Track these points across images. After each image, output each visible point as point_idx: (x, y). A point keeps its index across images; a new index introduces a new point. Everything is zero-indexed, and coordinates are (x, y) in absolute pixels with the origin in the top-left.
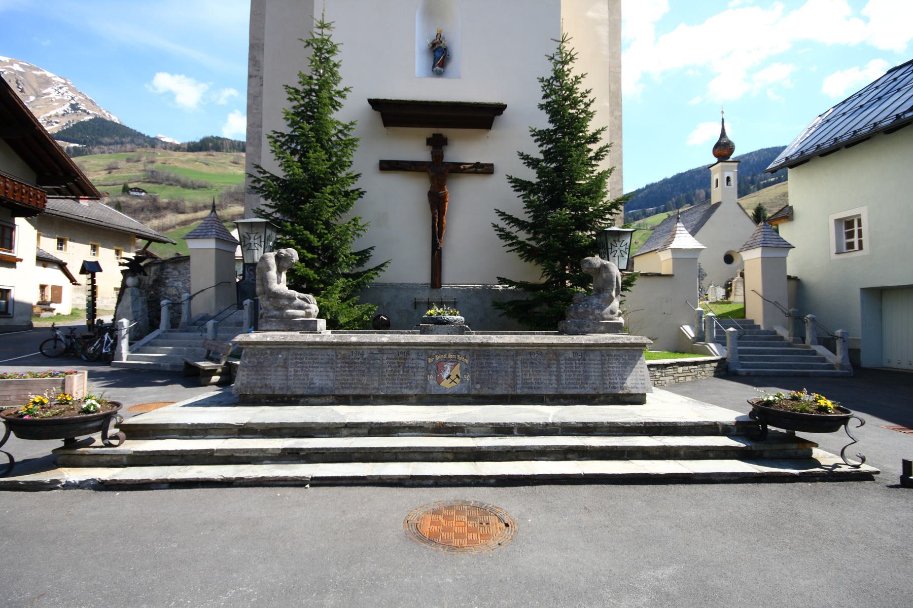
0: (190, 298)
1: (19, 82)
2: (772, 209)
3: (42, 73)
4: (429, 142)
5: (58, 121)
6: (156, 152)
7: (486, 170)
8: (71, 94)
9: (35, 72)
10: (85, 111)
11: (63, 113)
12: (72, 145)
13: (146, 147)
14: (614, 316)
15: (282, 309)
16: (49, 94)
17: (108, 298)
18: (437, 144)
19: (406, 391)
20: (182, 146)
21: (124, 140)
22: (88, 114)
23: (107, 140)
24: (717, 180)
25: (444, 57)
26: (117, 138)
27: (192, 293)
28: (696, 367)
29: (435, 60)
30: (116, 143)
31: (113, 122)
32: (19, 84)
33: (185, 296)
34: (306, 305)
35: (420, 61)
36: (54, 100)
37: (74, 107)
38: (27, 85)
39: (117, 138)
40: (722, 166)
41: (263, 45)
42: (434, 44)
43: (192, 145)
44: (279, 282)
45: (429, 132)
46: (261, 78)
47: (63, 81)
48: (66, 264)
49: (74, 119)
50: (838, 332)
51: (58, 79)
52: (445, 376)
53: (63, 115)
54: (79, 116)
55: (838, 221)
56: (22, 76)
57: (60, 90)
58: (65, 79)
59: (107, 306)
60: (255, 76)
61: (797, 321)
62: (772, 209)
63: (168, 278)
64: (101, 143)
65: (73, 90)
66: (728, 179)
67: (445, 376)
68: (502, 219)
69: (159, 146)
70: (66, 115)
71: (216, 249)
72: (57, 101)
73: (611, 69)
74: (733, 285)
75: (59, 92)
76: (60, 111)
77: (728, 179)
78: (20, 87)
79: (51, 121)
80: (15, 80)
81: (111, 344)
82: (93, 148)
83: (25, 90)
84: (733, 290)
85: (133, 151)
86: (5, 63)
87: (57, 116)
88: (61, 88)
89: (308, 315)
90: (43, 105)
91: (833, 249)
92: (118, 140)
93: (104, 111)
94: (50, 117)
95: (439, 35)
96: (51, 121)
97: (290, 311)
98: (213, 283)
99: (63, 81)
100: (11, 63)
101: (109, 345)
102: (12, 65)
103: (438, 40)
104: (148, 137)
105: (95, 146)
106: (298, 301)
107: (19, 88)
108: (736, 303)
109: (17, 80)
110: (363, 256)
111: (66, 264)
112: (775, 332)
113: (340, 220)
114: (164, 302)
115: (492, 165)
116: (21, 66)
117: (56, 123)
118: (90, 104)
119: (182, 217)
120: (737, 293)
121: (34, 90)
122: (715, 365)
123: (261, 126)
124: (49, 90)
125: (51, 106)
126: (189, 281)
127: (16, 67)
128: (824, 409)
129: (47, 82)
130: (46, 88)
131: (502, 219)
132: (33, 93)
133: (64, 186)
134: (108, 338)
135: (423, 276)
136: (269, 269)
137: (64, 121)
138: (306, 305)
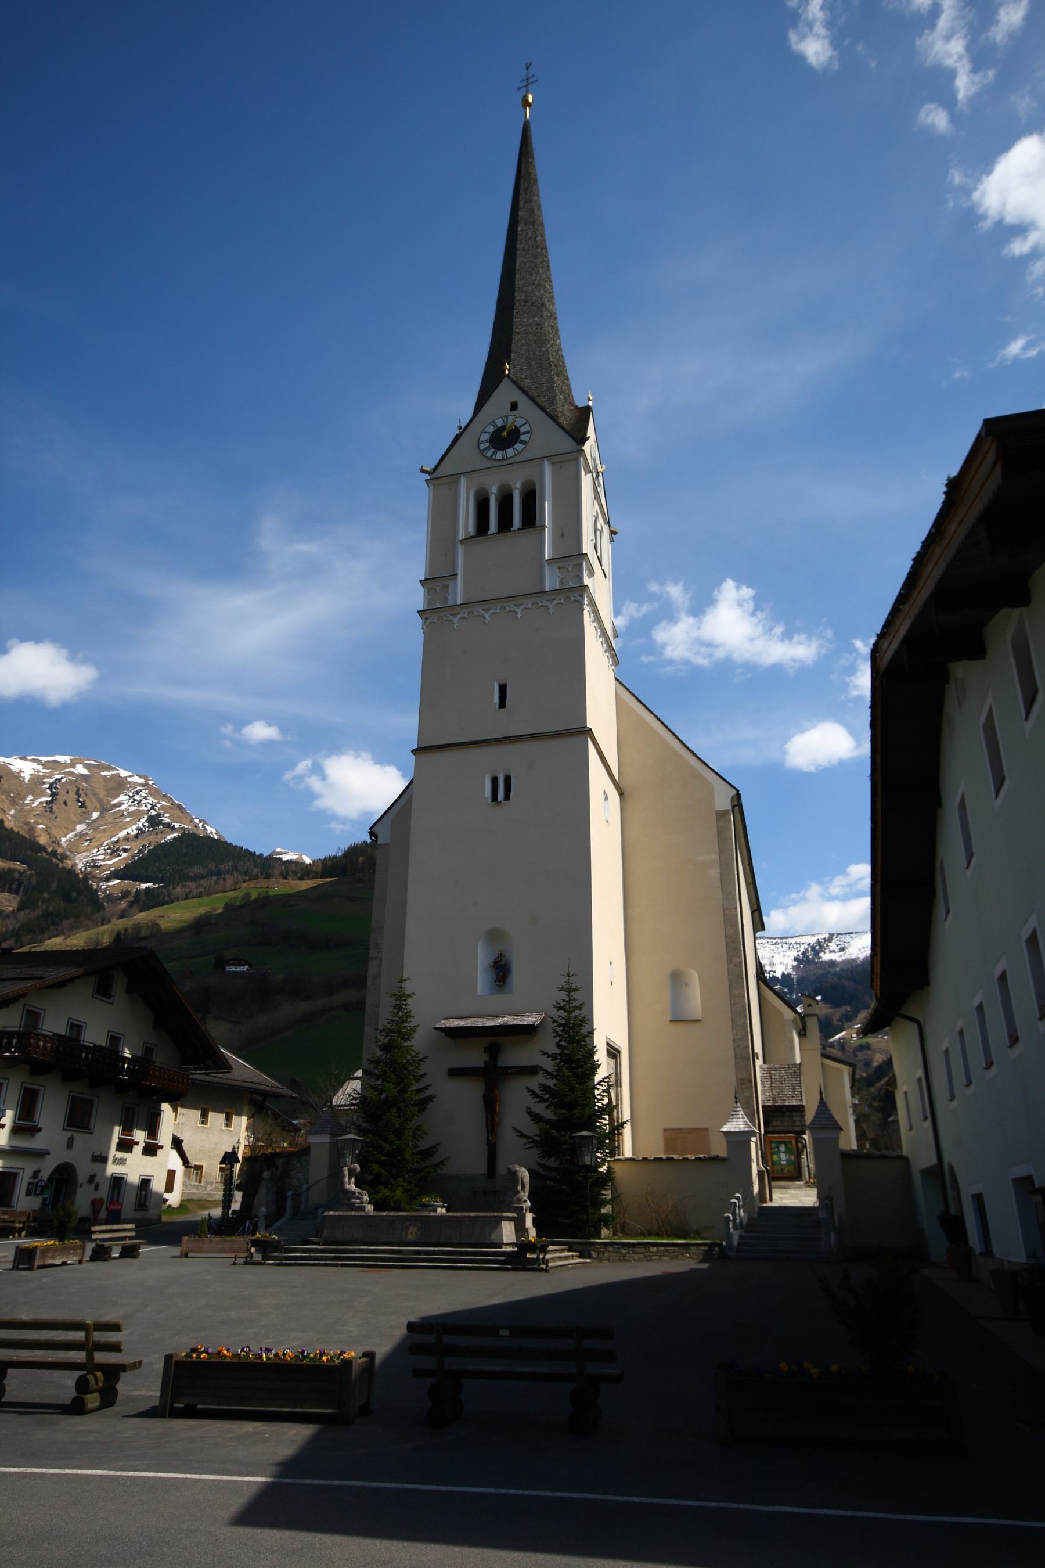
0: (308, 1189)
1: (81, 792)
3: (114, 772)
4: (486, 1050)
5: (127, 847)
6: (271, 885)
7: (532, 1071)
8: (151, 800)
9: (105, 773)
10: (168, 825)
11: (135, 832)
12: (144, 886)
13: (256, 878)
14: (520, 1202)
15: (349, 1199)
16: (120, 804)
17: (212, 1183)
18: (493, 1051)
19: (392, 1240)
20: (314, 869)
21: (222, 867)
22: (173, 829)
23: (197, 870)
25: (504, 973)
26: (212, 866)
27: (310, 1184)
28: (676, 1248)
29: (497, 975)
30: (211, 874)
31: (209, 839)
32: (79, 796)
33: (305, 1186)
34: (361, 1197)
35: (482, 980)
36: (125, 813)
37: (153, 821)
38: (90, 796)
39: (212, 866)
41: (384, 927)
42: (496, 963)
43: (329, 863)
44: (349, 1184)
46: (381, 959)
47: (142, 781)
48: (182, 1141)
49: (152, 840)
51: (136, 779)
52: (410, 1232)
53: (136, 836)
54: (160, 836)
56: (86, 782)
57: (137, 797)
58: (145, 778)
59: (209, 1195)
64: (186, 878)
65: (154, 793)
69: (276, 871)
70: (140, 837)
71: (330, 1143)
72: (130, 814)
73: (726, 912)
75: (135, 800)
76: (132, 830)
78: (81, 800)
79: (118, 849)
80: (75, 789)
81: (251, 1231)
82: (174, 888)
83: (88, 803)
85: (235, 889)
86: (65, 765)
87: (127, 839)
88: (138, 793)
89: (362, 1202)
90: (110, 823)
92: (214, 868)
93: (197, 821)
94: (117, 841)
95: (501, 955)
96: (118, 849)
97: (353, 1200)
98: (326, 1175)
99: (142, 781)
100: (73, 764)
101: (250, 1231)
102: (74, 767)
103: (499, 959)
104: (261, 855)
105: (178, 885)
106: (357, 1194)
107: (79, 801)
109: (78, 790)
110: (429, 1153)
111: (182, 1141)
113: (410, 1124)
114: (290, 1193)
116: (87, 766)
117: (125, 850)
118: (178, 812)
119: (306, 1006)
121: (100, 801)
122: (706, 1248)
123: (378, 1006)
124: (123, 798)
125: (120, 824)
126: (308, 1172)
127: (80, 769)
129: (119, 785)
130: (118, 796)
132: (98, 806)
133: (203, 1065)
135: (481, 1168)
136: (344, 1177)
137: (136, 847)
138: (361, 1197)
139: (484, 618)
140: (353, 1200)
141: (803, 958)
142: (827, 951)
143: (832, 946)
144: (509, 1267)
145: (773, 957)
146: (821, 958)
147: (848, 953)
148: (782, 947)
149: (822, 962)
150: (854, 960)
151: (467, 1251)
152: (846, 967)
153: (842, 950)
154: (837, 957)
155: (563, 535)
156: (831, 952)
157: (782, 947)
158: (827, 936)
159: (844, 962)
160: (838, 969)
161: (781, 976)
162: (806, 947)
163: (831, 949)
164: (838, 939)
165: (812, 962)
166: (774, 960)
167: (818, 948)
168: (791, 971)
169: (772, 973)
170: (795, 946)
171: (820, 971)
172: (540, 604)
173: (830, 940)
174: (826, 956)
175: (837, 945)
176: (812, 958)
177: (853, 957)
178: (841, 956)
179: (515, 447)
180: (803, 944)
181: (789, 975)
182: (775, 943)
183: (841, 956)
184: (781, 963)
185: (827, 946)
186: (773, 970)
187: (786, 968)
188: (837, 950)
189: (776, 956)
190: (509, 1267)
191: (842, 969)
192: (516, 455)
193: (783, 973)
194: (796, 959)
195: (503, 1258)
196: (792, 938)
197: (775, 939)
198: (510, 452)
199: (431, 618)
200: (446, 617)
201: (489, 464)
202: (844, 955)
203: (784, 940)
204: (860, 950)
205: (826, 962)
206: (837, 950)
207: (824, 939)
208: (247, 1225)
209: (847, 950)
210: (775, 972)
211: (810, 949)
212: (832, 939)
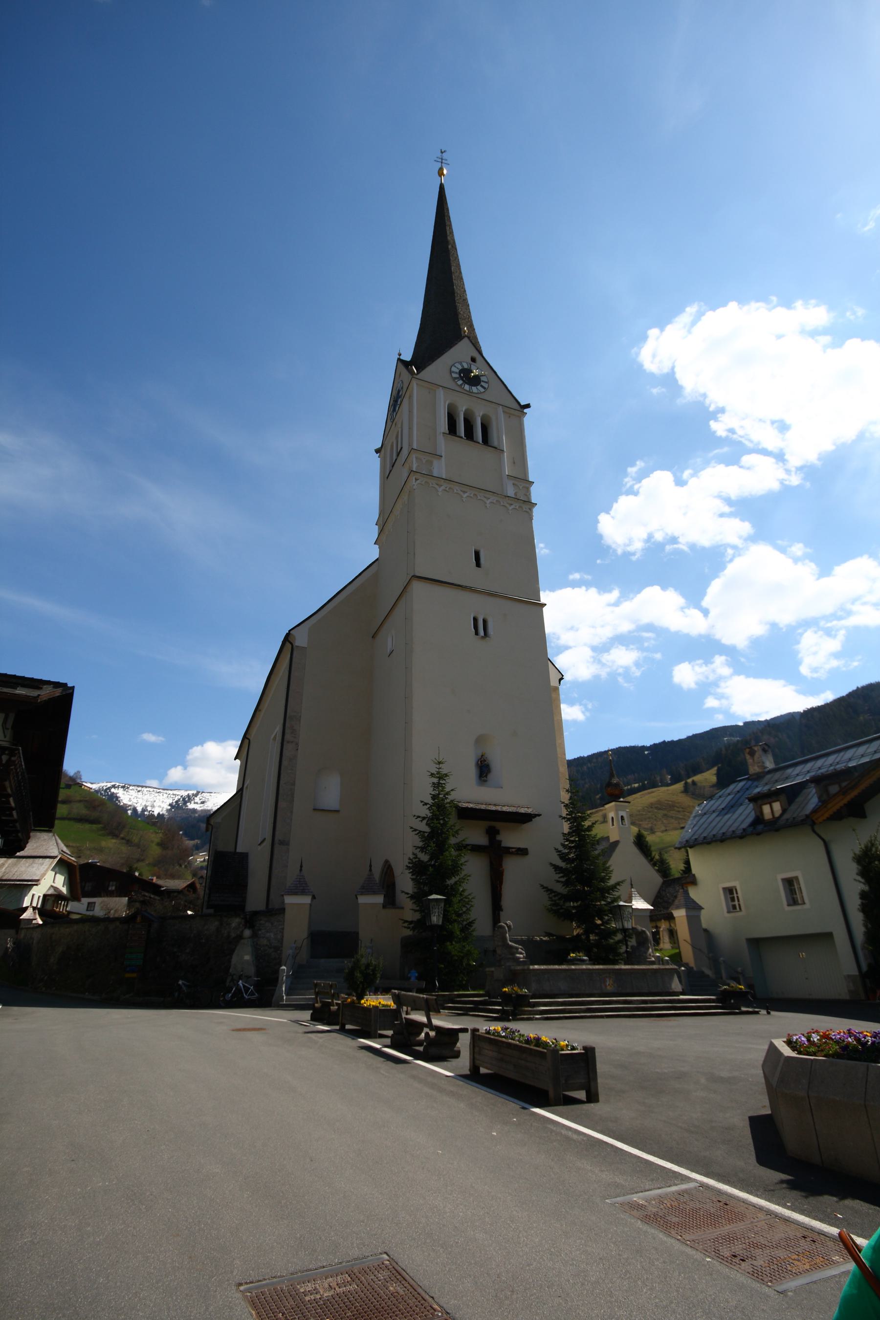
2: (641, 823)
18: (492, 833)
19: (595, 992)
24: (613, 818)
40: (615, 805)
45: (487, 824)
46: (297, 744)
50: (739, 969)
52: (607, 984)
55: (724, 889)
60: (292, 742)
61: (714, 961)
62: (641, 823)
63: (260, 930)
66: (622, 817)
67: (607, 984)
68: (544, 891)
74: (661, 933)
77: (622, 817)
84: (661, 938)
91: (725, 910)
97: (518, 955)
108: (666, 950)
112: (703, 972)
115: (527, 849)
120: (665, 941)
123: (294, 784)
128: (741, 989)
131: (544, 891)
134: (243, 984)
139: (486, 503)
140: (518, 955)
141: (176, 804)
142: (192, 802)
143: (197, 799)
144: (737, 1011)
145: (155, 801)
146: (187, 806)
147: (206, 806)
148: (163, 795)
149: (187, 809)
150: (209, 811)
151: (545, 1001)
152: (203, 815)
153: (203, 803)
154: (198, 807)
155: (514, 463)
156: (195, 803)
157: (163, 795)
158: (195, 792)
159: (202, 810)
160: (197, 815)
161: (157, 815)
162: (179, 797)
163: (196, 801)
164: (202, 795)
165: (181, 808)
166: (155, 803)
167: (189, 799)
168: (164, 812)
169: (151, 812)
170: (172, 796)
171: (184, 815)
172: (502, 504)
173: (196, 795)
174: (191, 806)
175: (200, 800)
176: (182, 805)
177: (209, 808)
178: (201, 807)
179: (473, 387)
180: (178, 795)
181: (163, 815)
182: (159, 792)
183: (201, 807)
184: (160, 806)
185: (194, 799)
186: (153, 810)
187: (162, 810)
188: (199, 803)
189: (157, 801)
190: (737, 1011)
191: (199, 816)
192: (478, 393)
193: (159, 813)
194: (170, 805)
195: (480, 1007)
196: (171, 790)
197: (159, 789)
198: (474, 389)
199: (420, 480)
200: (432, 484)
201: (458, 389)
202: (203, 806)
203: (165, 791)
204: (214, 804)
205: (190, 809)
206: (199, 802)
207: (193, 794)
208: (241, 985)
209: (205, 804)
210: (153, 812)
211: (181, 799)
212: (198, 795)
